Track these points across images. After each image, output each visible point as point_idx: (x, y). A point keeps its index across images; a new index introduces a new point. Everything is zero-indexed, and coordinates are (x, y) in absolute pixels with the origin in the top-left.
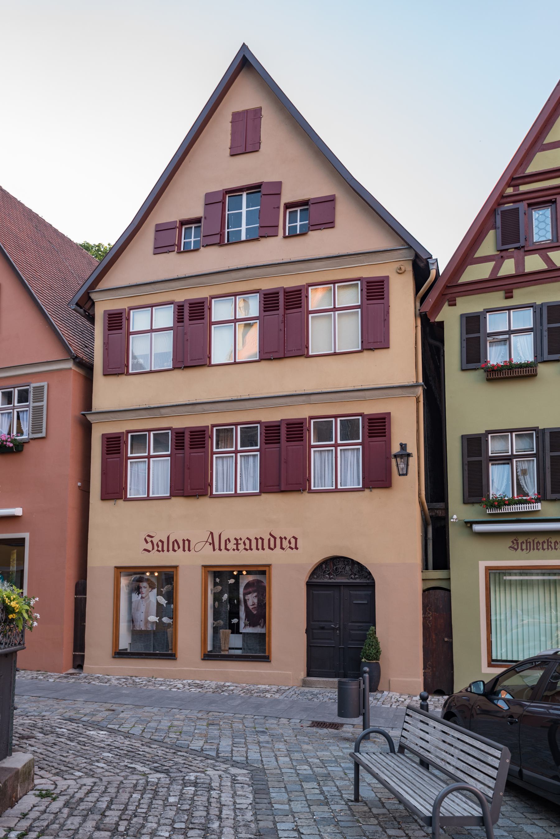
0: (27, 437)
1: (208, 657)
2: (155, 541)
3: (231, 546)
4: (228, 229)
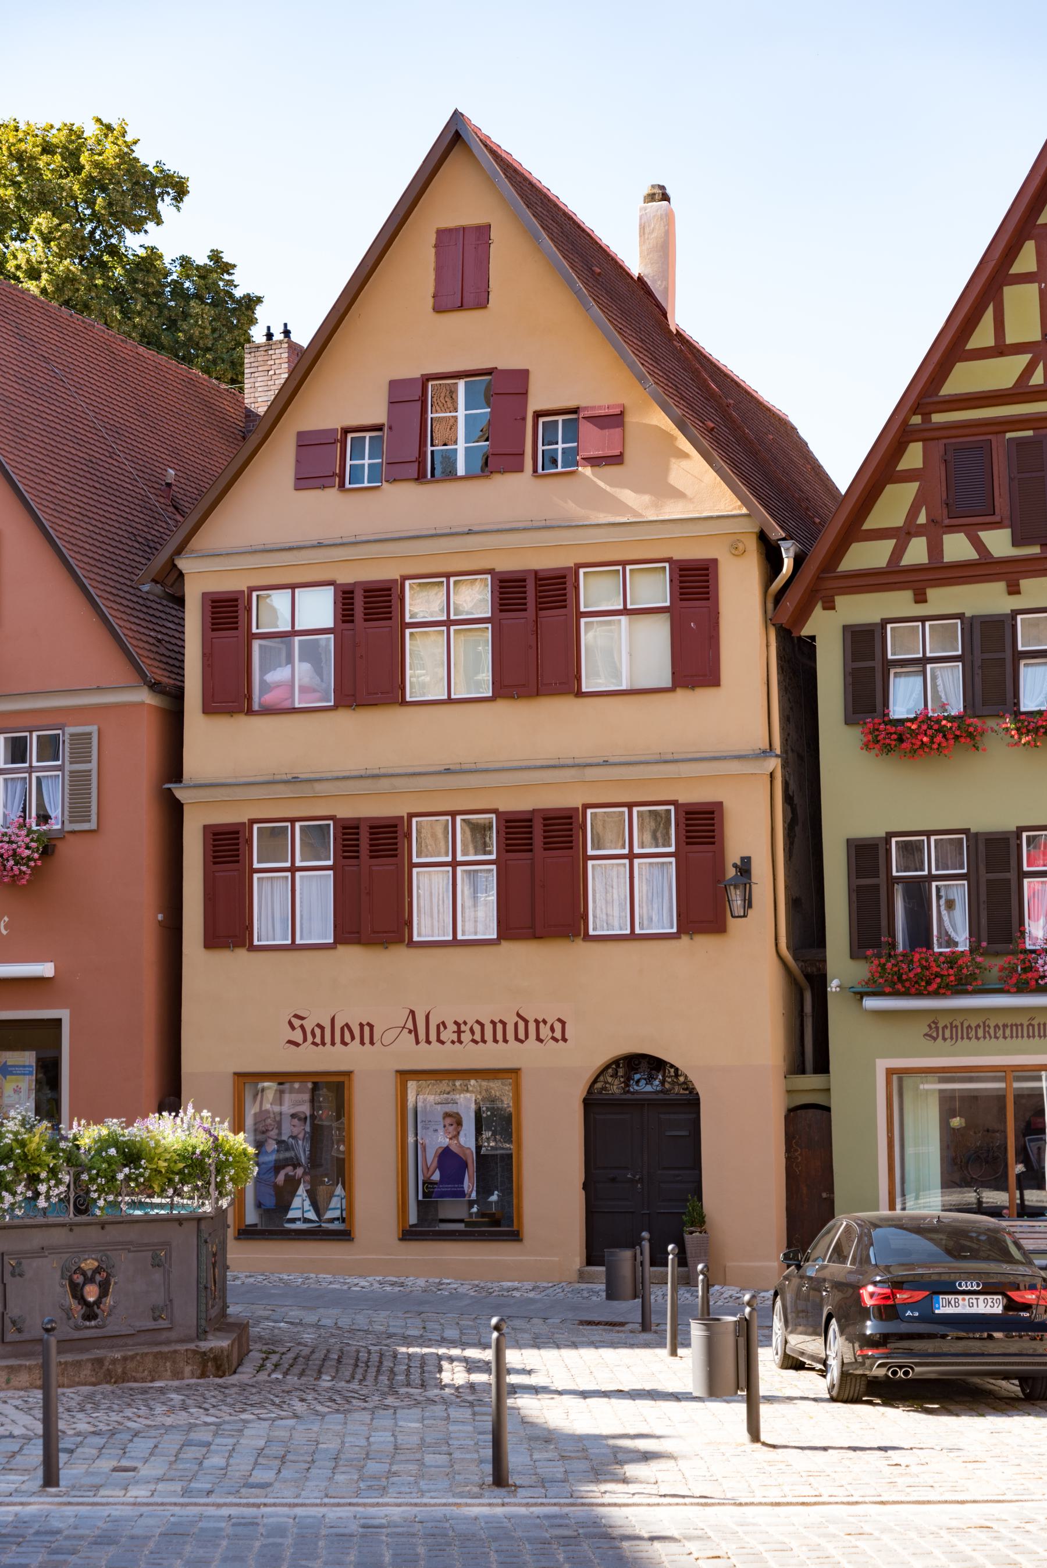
0: (59, 827)
1: (408, 1235)
2: (309, 1025)
3: (448, 1035)
4: (432, 445)
